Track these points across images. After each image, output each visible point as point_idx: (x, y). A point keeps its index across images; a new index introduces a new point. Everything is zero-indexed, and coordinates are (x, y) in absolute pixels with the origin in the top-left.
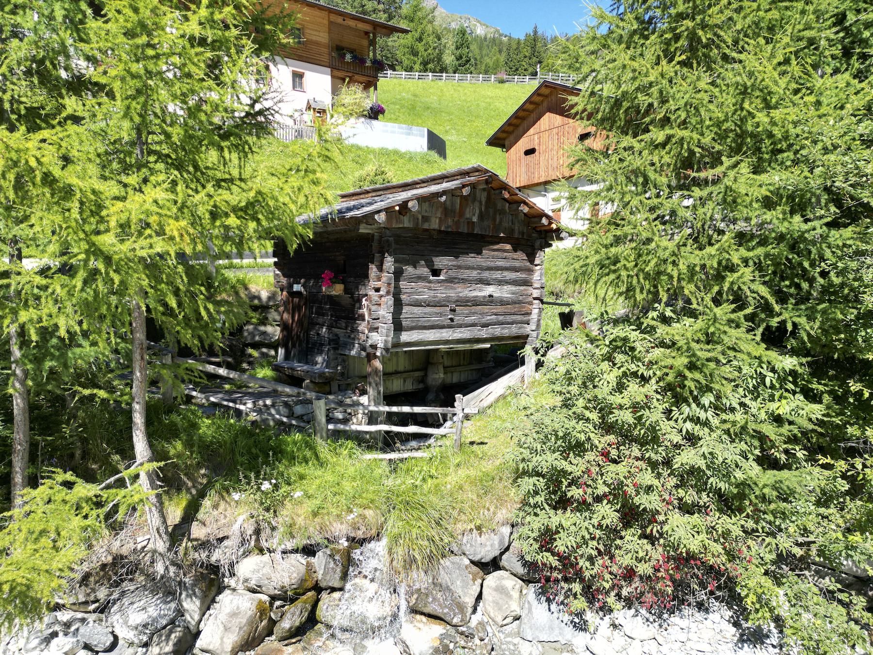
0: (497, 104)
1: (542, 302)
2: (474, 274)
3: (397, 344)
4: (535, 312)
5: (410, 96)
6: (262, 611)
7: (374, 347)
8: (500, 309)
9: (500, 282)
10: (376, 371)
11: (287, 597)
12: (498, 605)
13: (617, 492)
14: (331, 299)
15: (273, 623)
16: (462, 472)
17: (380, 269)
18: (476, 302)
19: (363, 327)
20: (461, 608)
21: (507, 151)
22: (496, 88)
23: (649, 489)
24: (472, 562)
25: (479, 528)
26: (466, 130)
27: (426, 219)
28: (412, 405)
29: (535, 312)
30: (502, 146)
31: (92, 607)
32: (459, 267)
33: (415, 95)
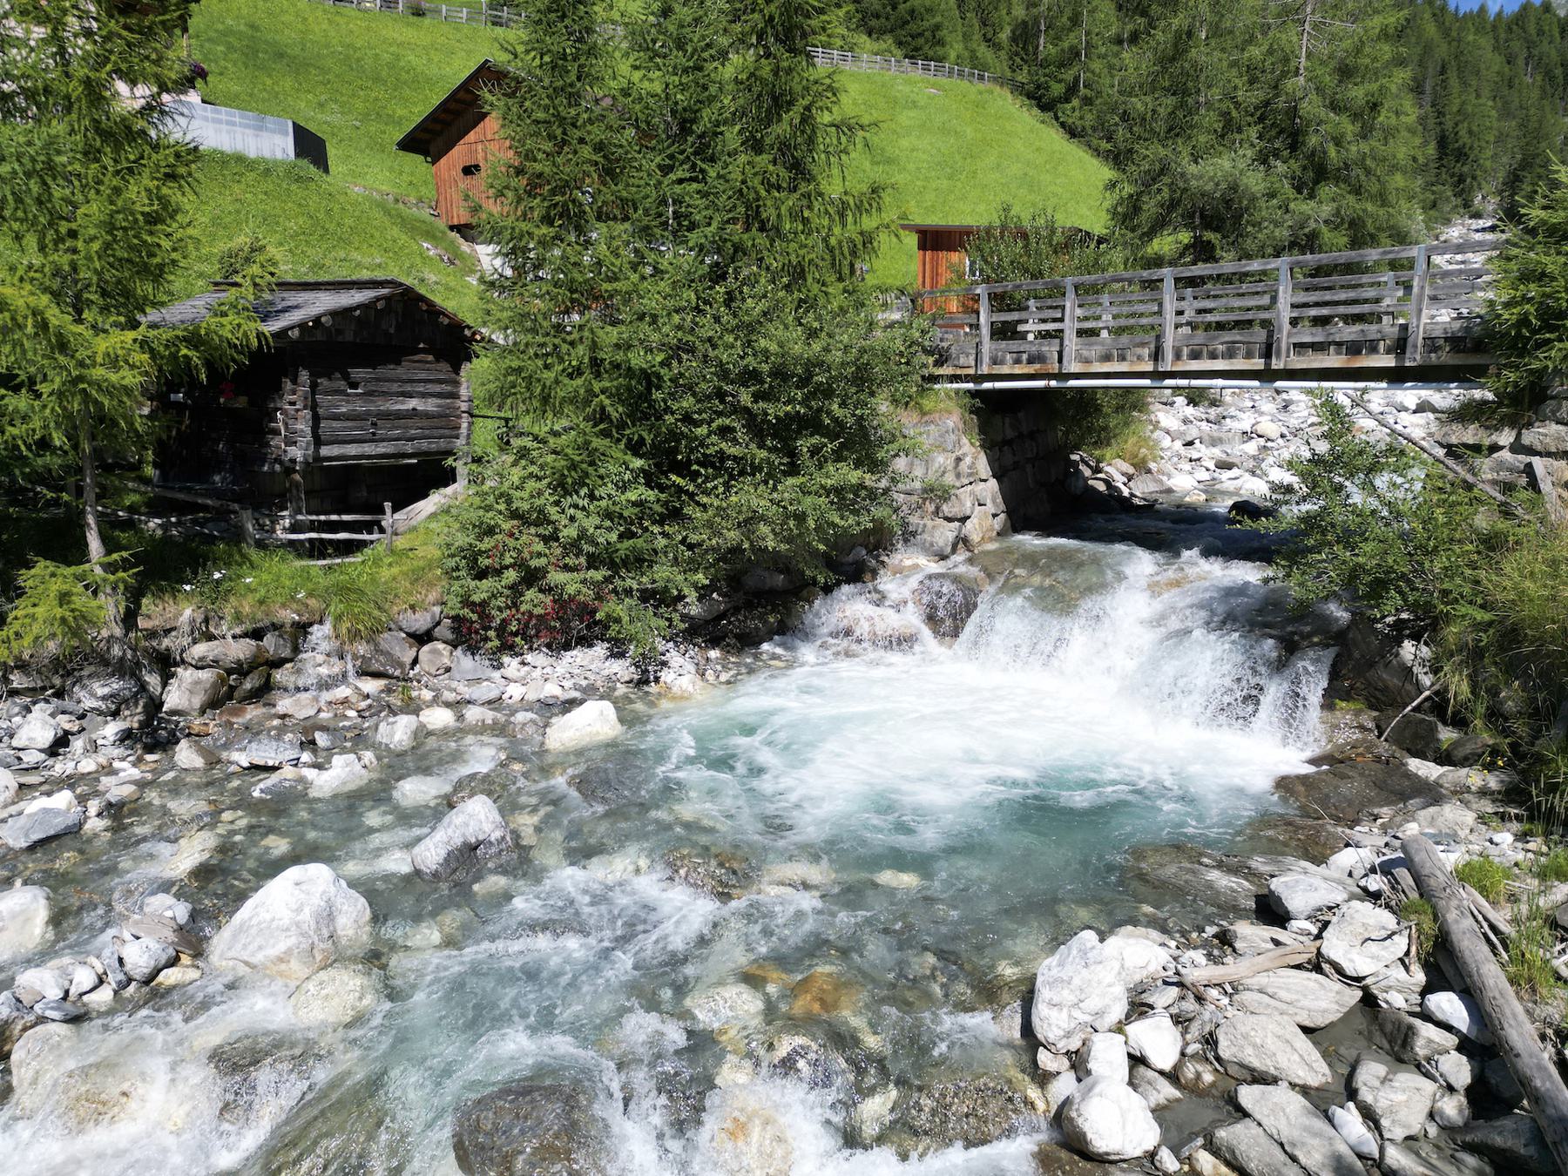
0: (411, 58)
1: (472, 416)
2: (395, 387)
3: (318, 458)
4: (465, 425)
5: (242, 28)
6: (222, 681)
7: (293, 461)
8: (425, 423)
9: (424, 395)
10: (297, 485)
11: (241, 669)
12: (431, 662)
13: (520, 564)
14: (177, 403)
15: (232, 689)
16: (395, 570)
17: (294, 382)
18: (399, 415)
19: (276, 441)
20: (401, 665)
21: (433, 163)
22: (408, 24)
23: (539, 555)
24: (409, 635)
25: (413, 607)
26: (359, 105)
27: (339, 332)
28: (339, 514)
29: (465, 425)
30: (425, 153)
31: (50, 692)
32: (378, 380)
33: (253, 26)
